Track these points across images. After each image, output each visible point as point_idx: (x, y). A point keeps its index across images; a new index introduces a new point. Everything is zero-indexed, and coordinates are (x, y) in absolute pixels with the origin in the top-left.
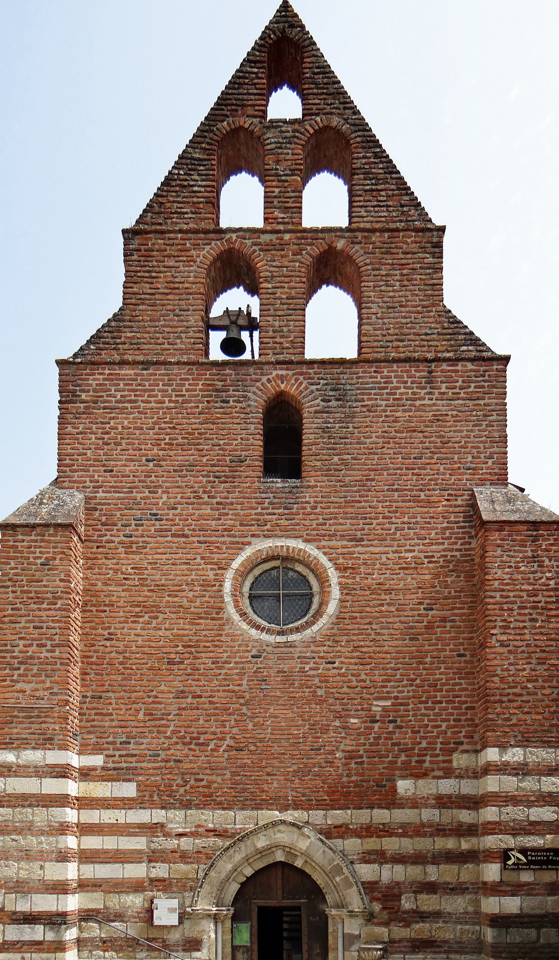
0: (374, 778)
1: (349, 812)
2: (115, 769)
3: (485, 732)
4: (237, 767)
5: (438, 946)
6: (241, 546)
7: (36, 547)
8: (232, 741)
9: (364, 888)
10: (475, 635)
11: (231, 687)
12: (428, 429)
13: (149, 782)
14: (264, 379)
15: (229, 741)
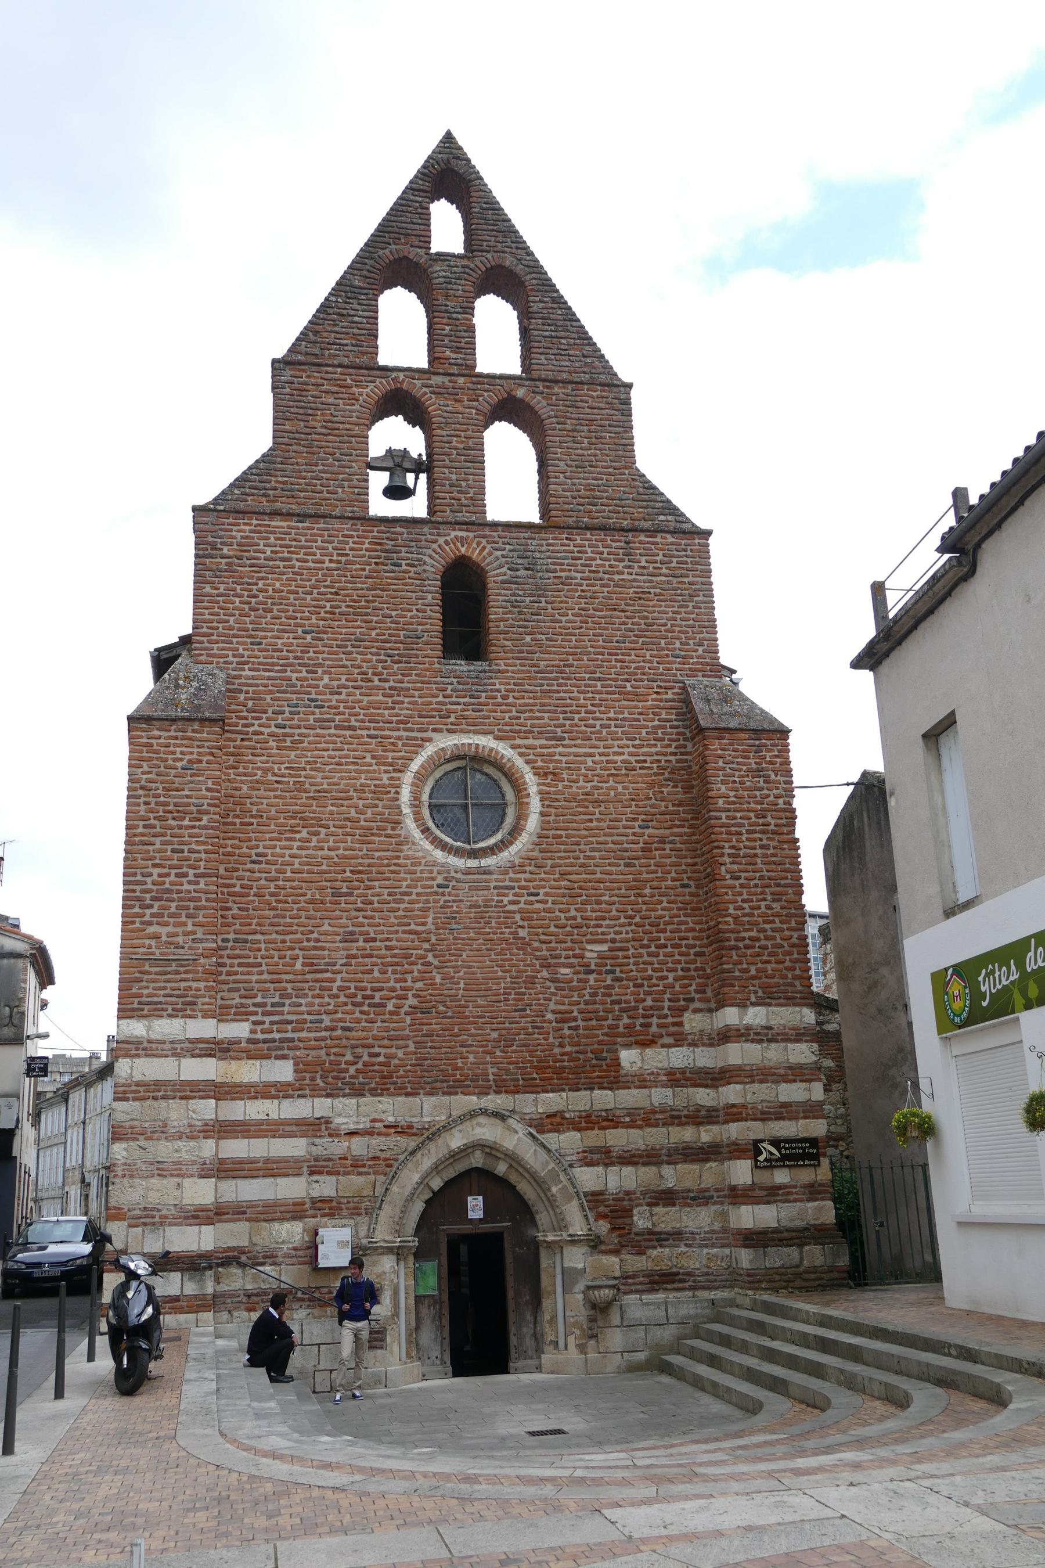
1: (564, 1094)
2: (265, 1041)
3: (720, 987)
5: (681, 1281)
11: (413, 927)
12: (630, 608)
14: (441, 540)
15: (412, 1001)
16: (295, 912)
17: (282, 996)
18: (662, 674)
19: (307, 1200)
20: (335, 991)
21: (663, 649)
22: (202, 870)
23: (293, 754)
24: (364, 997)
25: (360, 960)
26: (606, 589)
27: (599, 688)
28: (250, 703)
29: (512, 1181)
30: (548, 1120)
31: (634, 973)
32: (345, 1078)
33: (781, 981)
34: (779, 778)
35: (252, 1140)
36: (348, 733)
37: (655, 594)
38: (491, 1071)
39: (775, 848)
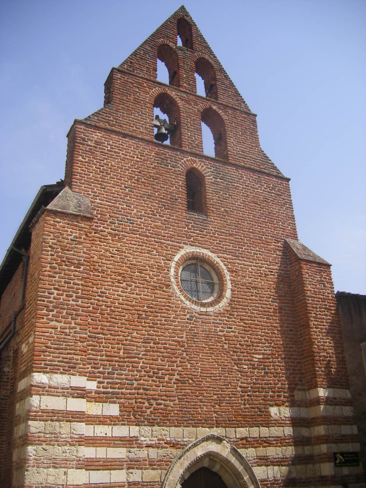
1: (247, 429)
2: (104, 393)
14: (185, 159)
19: (126, 483)
20: (140, 368)
24: (154, 373)
37: (271, 200)
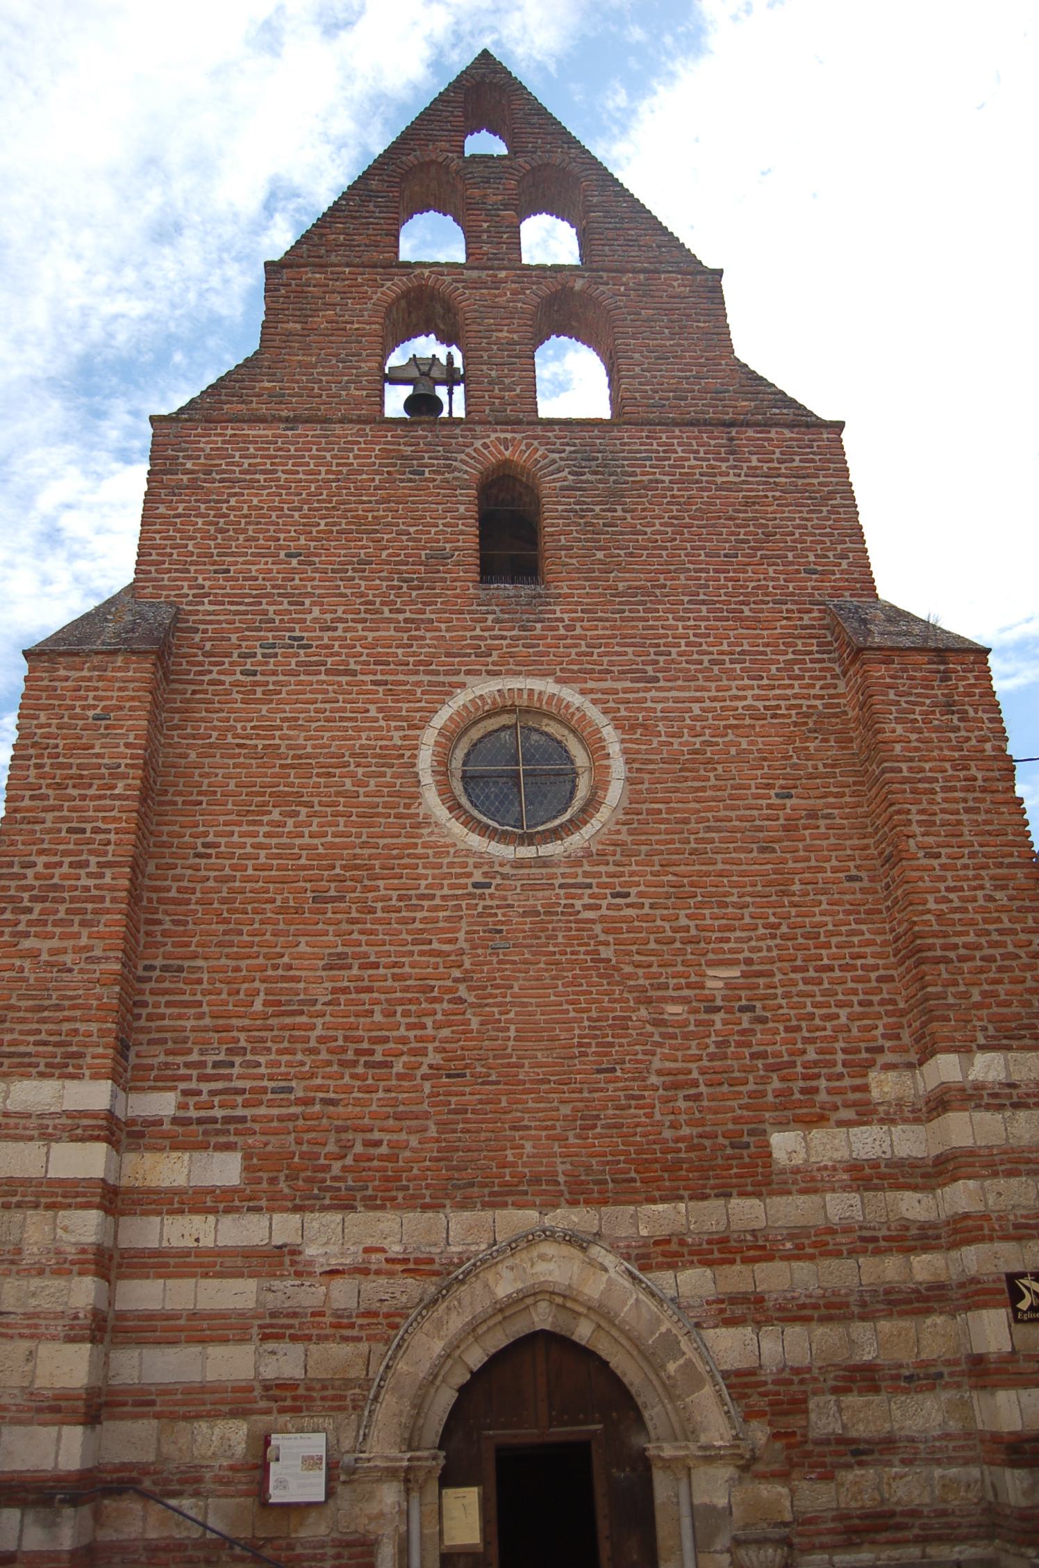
0: (724, 1128)
1: (682, 1206)
2: (200, 1121)
3: (924, 1025)
4: (450, 1112)
5: (899, 1527)
6: (447, 692)
7: (88, 689)
8: (438, 1056)
9: (728, 1387)
10: (871, 841)
11: (435, 946)
12: (741, 515)
13: (269, 1148)
14: (478, 444)
15: (433, 1058)
16: (256, 926)
17: (230, 1051)
18: (792, 594)
20: (313, 1044)
21: (792, 563)
22: (110, 858)
23: (265, 708)
24: (359, 1052)
25: (353, 996)
26: (706, 494)
27: (704, 613)
28: (208, 646)
29: (603, 1354)
30: (659, 1249)
31: (785, 1011)
32: (324, 1180)
33: (1023, 1011)
34: (980, 714)
35: (170, 1282)
36: (344, 679)
38: (560, 1168)
39: (988, 812)
